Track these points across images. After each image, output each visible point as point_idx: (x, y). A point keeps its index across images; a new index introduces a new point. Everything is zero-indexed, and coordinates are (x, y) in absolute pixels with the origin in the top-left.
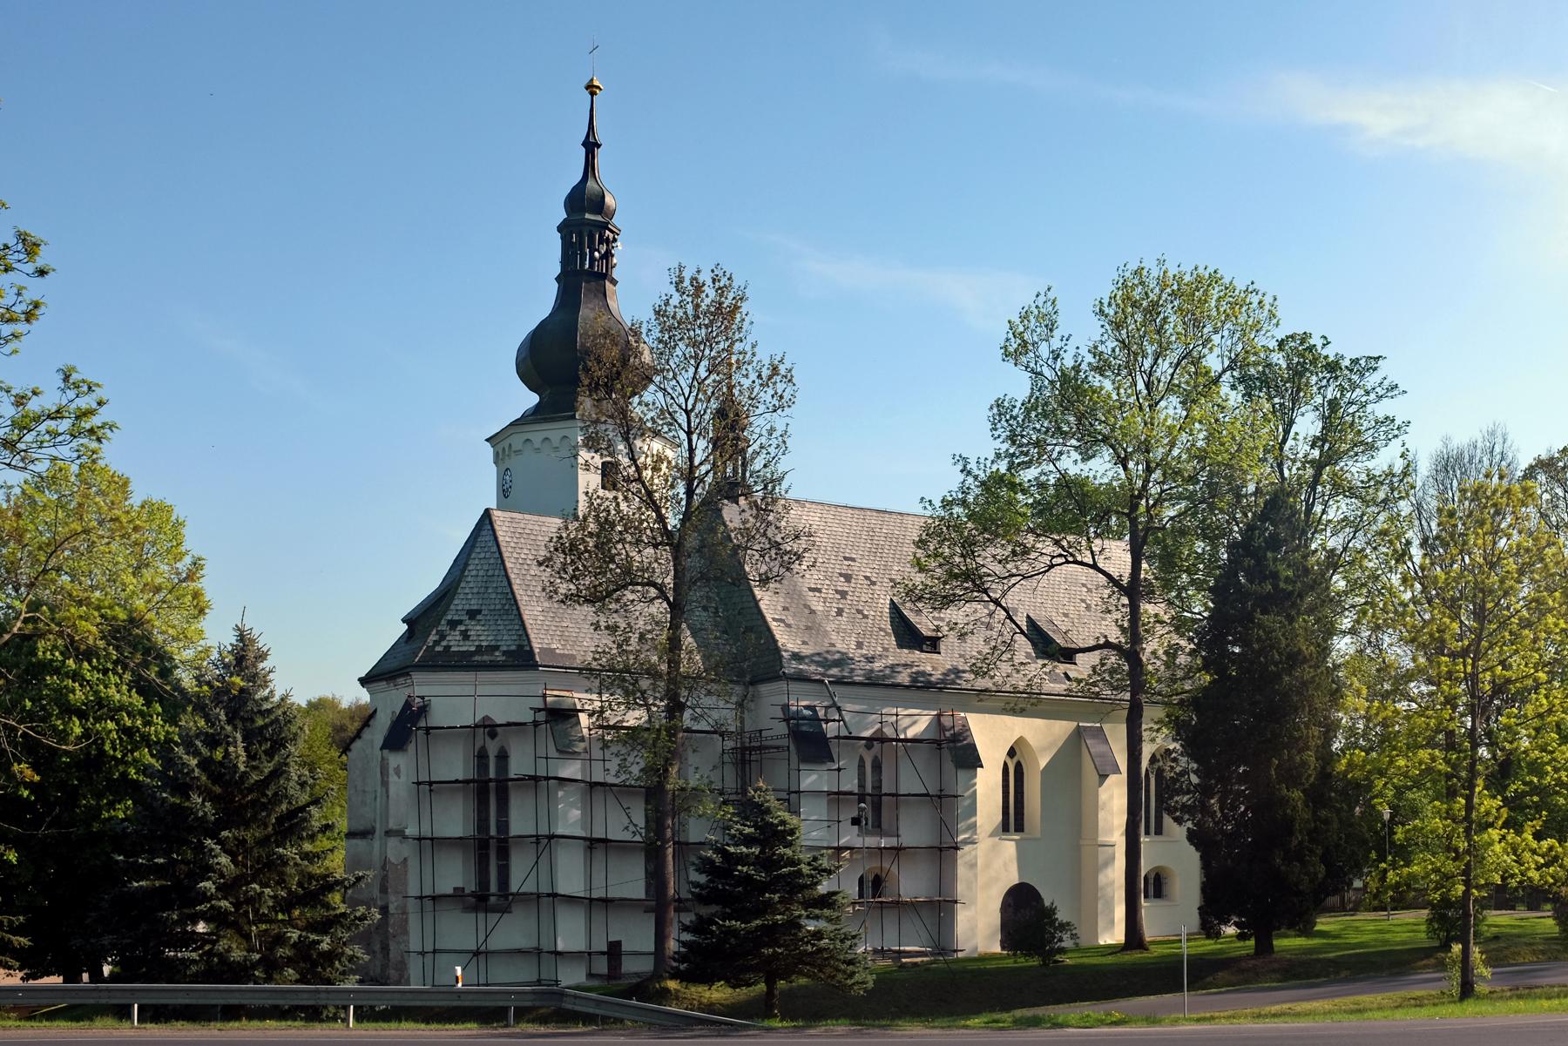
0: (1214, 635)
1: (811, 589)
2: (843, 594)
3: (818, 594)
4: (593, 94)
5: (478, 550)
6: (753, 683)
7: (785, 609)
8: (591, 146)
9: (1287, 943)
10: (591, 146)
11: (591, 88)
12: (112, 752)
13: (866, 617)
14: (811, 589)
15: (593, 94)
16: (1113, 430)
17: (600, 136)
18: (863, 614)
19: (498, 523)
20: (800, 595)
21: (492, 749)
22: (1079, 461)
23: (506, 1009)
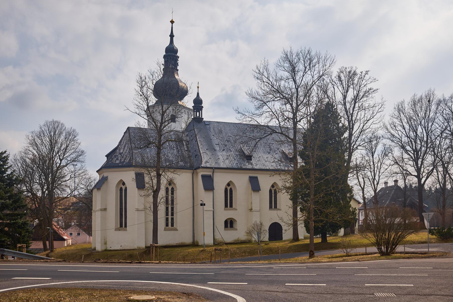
0: (293, 197)
1: (216, 144)
2: (226, 146)
3: (218, 146)
4: (172, 24)
5: (125, 137)
6: (195, 169)
7: (207, 150)
8: (172, 36)
9: (330, 239)
10: (172, 36)
11: (172, 22)
12: (59, 172)
13: (231, 151)
14: (216, 144)
15: (172, 24)
16: (40, 298)
17: (174, 33)
18: (231, 150)
19: (131, 130)
20: (213, 146)
21: (124, 188)
22: (348, 68)
23: (168, 216)
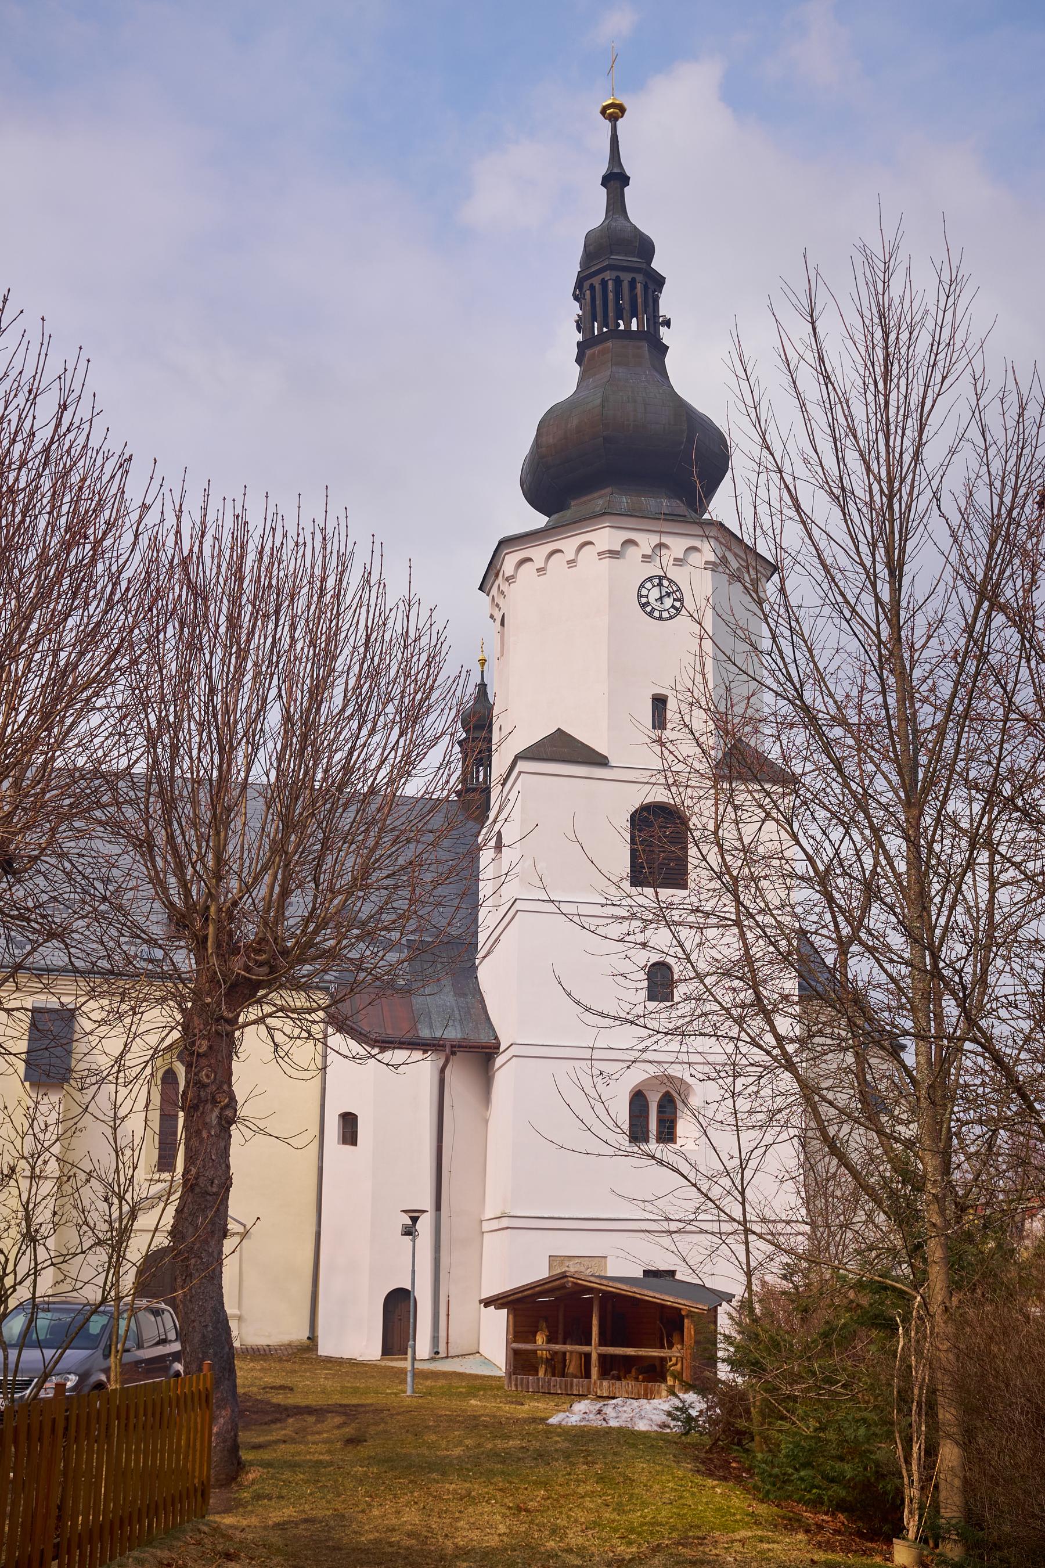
4: (613, 119)
15: (613, 119)
